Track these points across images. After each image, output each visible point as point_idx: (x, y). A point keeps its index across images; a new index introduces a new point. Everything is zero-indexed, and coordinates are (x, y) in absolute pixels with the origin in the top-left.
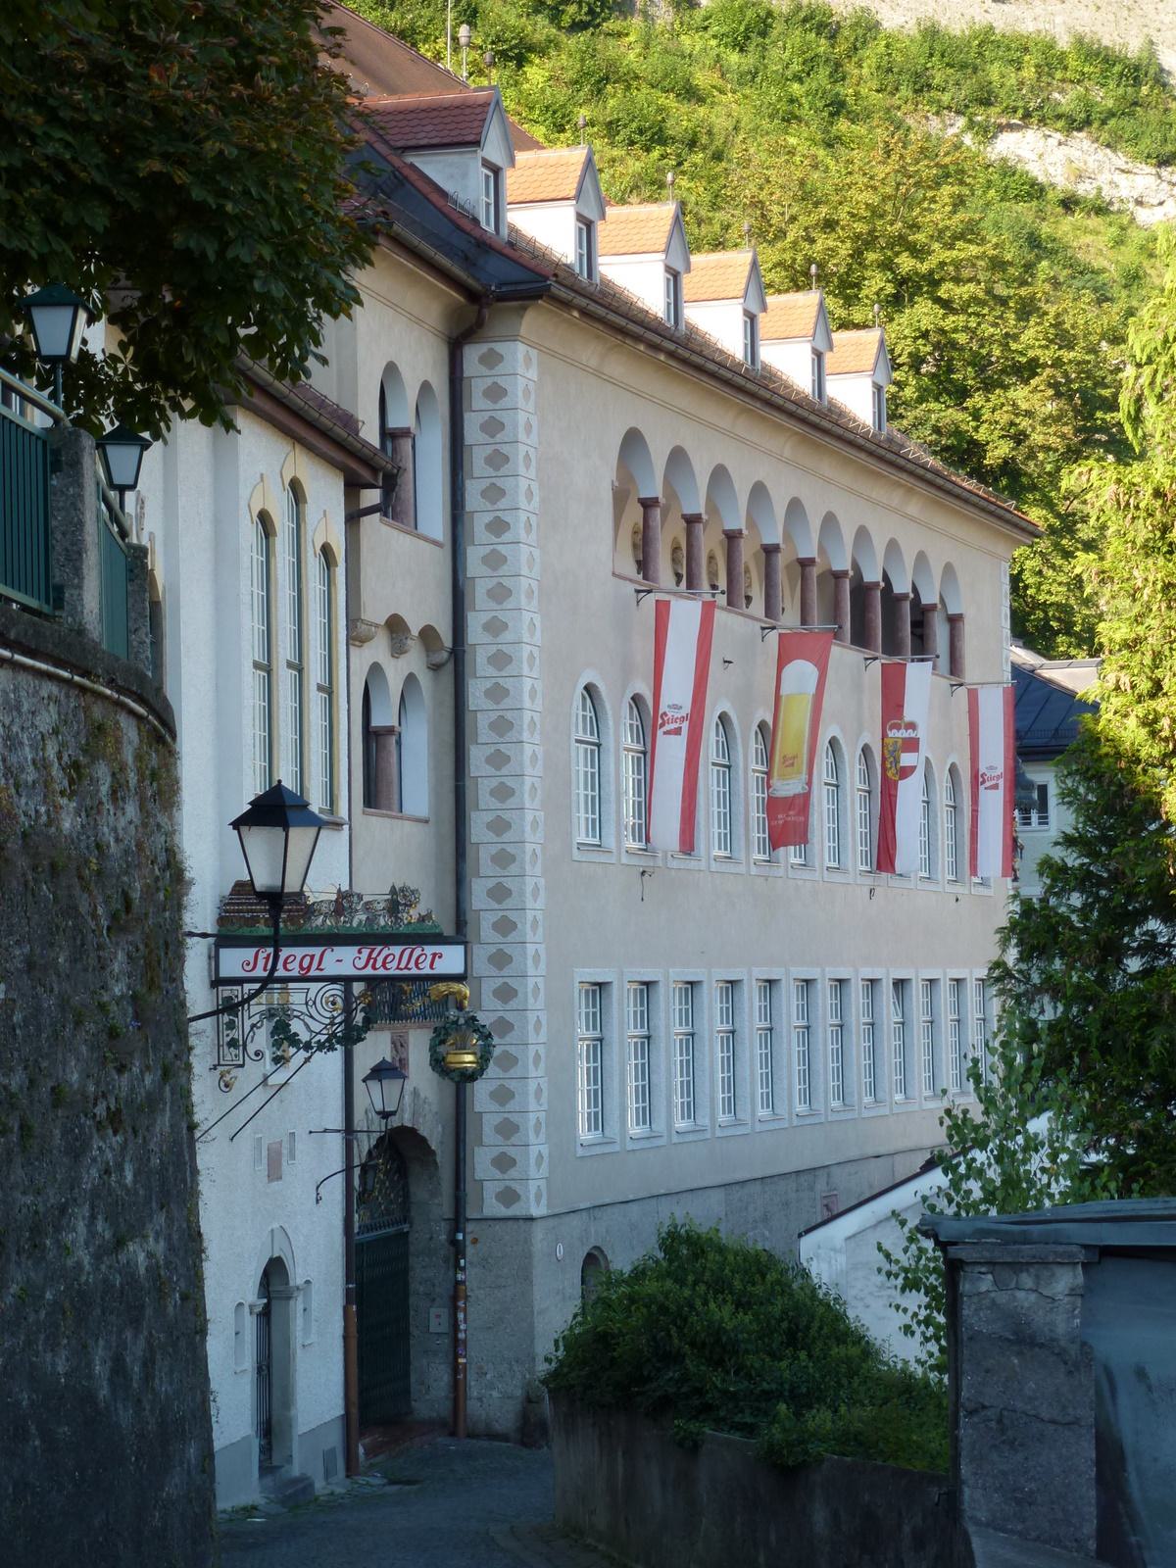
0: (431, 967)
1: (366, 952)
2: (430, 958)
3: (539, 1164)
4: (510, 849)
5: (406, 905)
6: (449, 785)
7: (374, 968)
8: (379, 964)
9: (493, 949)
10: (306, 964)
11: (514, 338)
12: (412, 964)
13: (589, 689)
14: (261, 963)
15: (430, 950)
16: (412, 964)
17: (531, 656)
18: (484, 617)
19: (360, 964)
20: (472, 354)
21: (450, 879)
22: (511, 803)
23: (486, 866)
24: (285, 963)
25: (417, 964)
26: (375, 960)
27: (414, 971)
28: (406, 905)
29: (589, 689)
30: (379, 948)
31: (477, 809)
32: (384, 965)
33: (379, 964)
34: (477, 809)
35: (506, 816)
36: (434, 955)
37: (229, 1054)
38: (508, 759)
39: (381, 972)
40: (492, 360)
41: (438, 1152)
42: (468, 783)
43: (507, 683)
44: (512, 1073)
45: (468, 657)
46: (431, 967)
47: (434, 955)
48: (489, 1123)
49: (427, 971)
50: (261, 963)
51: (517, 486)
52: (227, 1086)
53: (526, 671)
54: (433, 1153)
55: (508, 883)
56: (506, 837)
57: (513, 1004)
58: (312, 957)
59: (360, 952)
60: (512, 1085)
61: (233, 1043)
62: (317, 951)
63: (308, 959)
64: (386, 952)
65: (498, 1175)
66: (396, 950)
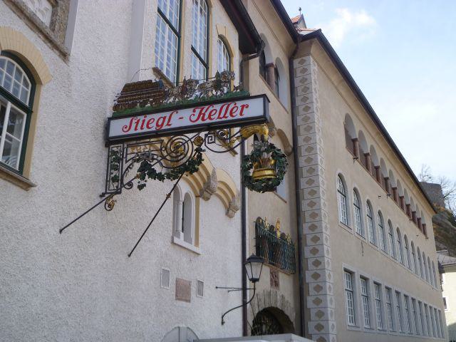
0: (241, 114)
1: (198, 111)
2: (240, 108)
3: (333, 329)
4: (316, 212)
5: (225, 82)
6: (294, 192)
7: (203, 119)
8: (206, 117)
9: (311, 248)
10: (160, 123)
11: (309, 54)
12: (228, 114)
13: (340, 176)
14: (134, 125)
15: (239, 104)
16: (228, 114)
17: (330, 287)
18: (303, 137)
19: (194, 118)
20: (296, 62)
21: (295, 224)
22: (316, 196)
23: (308, 218)
24: (148, 124)
25: (231, 114)
26: (204, 114)
27: (230, 118)
28: (225, 82)
29: (340, 176)
30: (207, 107)
31: (305, 222)
32: (209, 117)
33: (206, 117)
34: (305, 222)
35: (314, 200)
36: (243, 106)
37: (113, 186)
38: (318, 250)
39: (208, 121)
40: (302, 62)
41: (294, 323)
42: (301, 191)
43: (313, 157)
44: (320, 293)
45: (298, 151)
46: (241, 114)
47: (243, 106)
48: (313, 313)
49: (238, 117)
50: (134, 125)
51: (323, 249)
52: (110, 205)
53: (328, 293)
54: (292, 323)
55: (316, 224)
56: (316, 231)
57: (320, 267)
58: (164, 118)
59: (194, 111)
60: (321, 297)
61: (115, 179)
62: (167, 114)
63: (162, 120)
64: (211, 108)
65: (317, 332)
66: (218, 107)
